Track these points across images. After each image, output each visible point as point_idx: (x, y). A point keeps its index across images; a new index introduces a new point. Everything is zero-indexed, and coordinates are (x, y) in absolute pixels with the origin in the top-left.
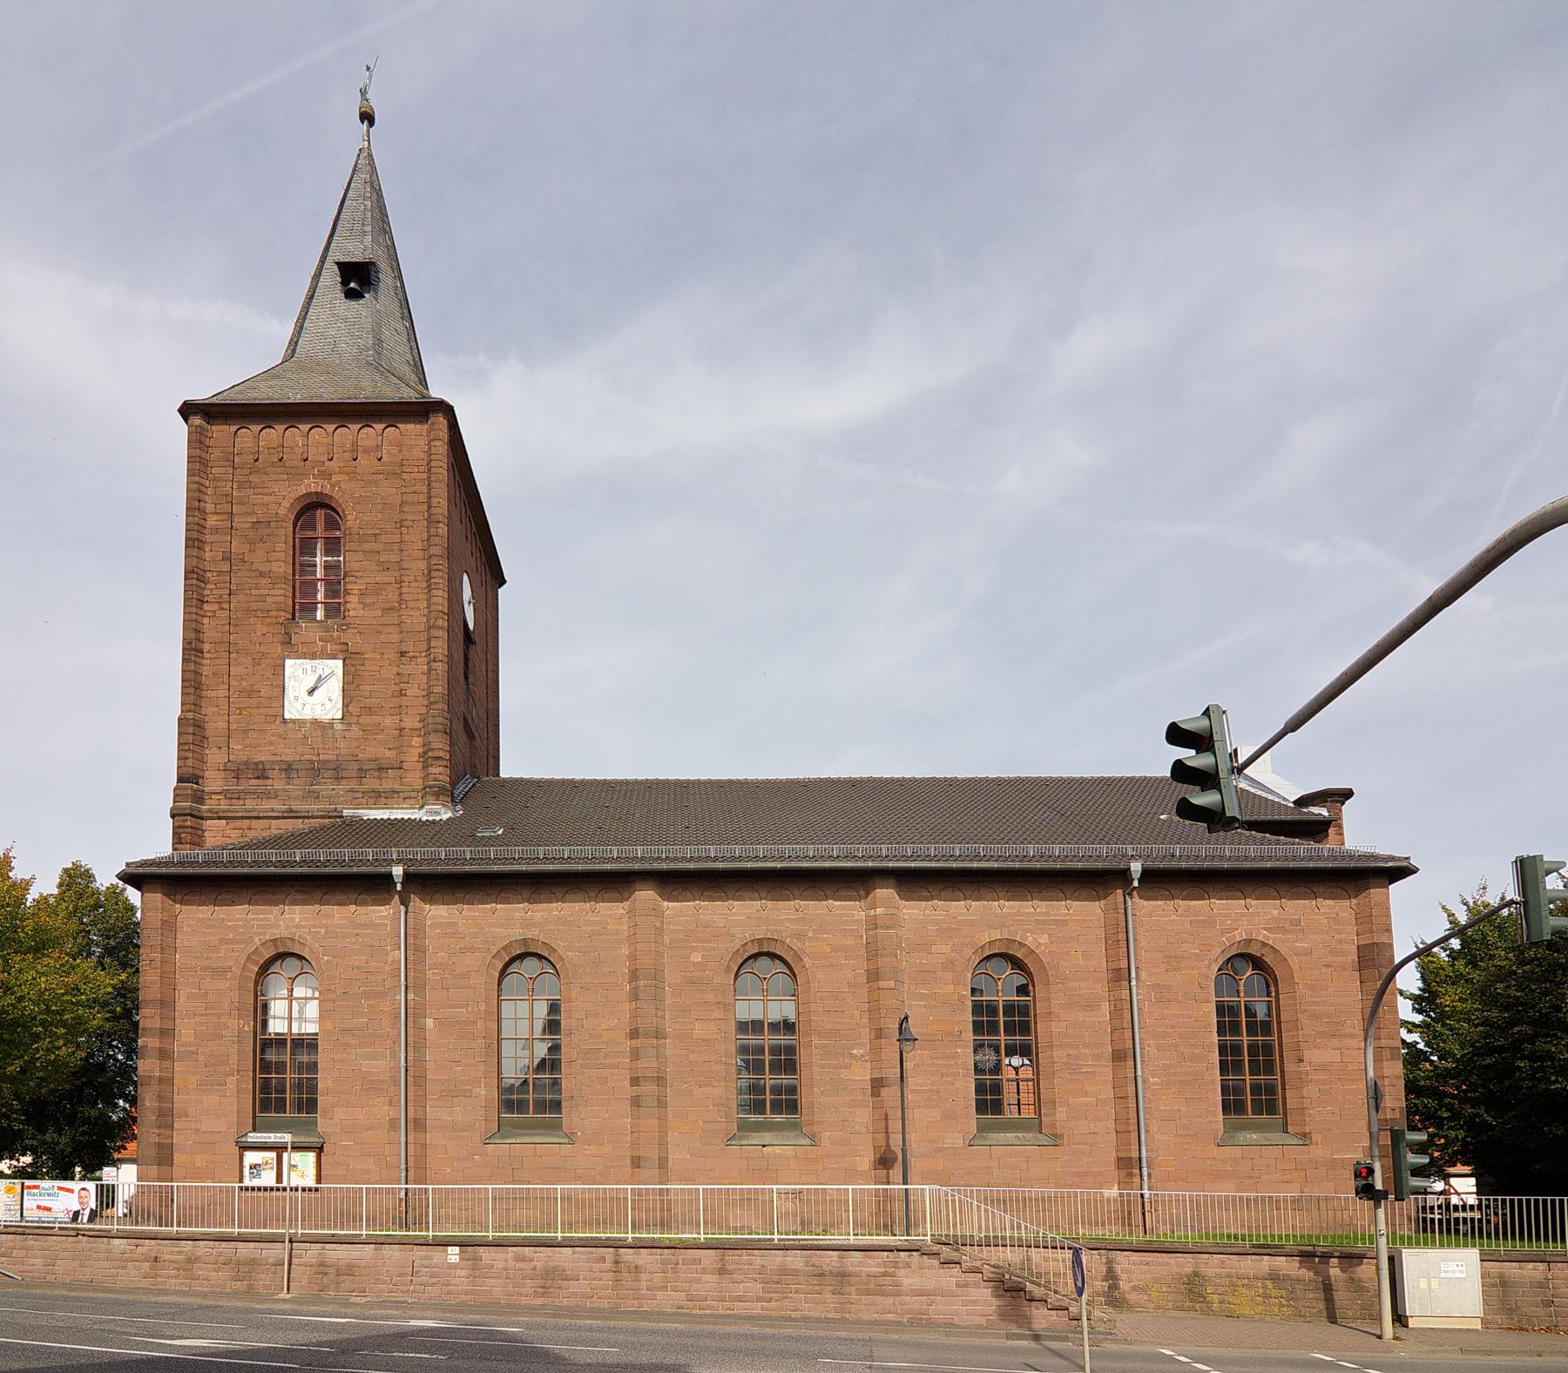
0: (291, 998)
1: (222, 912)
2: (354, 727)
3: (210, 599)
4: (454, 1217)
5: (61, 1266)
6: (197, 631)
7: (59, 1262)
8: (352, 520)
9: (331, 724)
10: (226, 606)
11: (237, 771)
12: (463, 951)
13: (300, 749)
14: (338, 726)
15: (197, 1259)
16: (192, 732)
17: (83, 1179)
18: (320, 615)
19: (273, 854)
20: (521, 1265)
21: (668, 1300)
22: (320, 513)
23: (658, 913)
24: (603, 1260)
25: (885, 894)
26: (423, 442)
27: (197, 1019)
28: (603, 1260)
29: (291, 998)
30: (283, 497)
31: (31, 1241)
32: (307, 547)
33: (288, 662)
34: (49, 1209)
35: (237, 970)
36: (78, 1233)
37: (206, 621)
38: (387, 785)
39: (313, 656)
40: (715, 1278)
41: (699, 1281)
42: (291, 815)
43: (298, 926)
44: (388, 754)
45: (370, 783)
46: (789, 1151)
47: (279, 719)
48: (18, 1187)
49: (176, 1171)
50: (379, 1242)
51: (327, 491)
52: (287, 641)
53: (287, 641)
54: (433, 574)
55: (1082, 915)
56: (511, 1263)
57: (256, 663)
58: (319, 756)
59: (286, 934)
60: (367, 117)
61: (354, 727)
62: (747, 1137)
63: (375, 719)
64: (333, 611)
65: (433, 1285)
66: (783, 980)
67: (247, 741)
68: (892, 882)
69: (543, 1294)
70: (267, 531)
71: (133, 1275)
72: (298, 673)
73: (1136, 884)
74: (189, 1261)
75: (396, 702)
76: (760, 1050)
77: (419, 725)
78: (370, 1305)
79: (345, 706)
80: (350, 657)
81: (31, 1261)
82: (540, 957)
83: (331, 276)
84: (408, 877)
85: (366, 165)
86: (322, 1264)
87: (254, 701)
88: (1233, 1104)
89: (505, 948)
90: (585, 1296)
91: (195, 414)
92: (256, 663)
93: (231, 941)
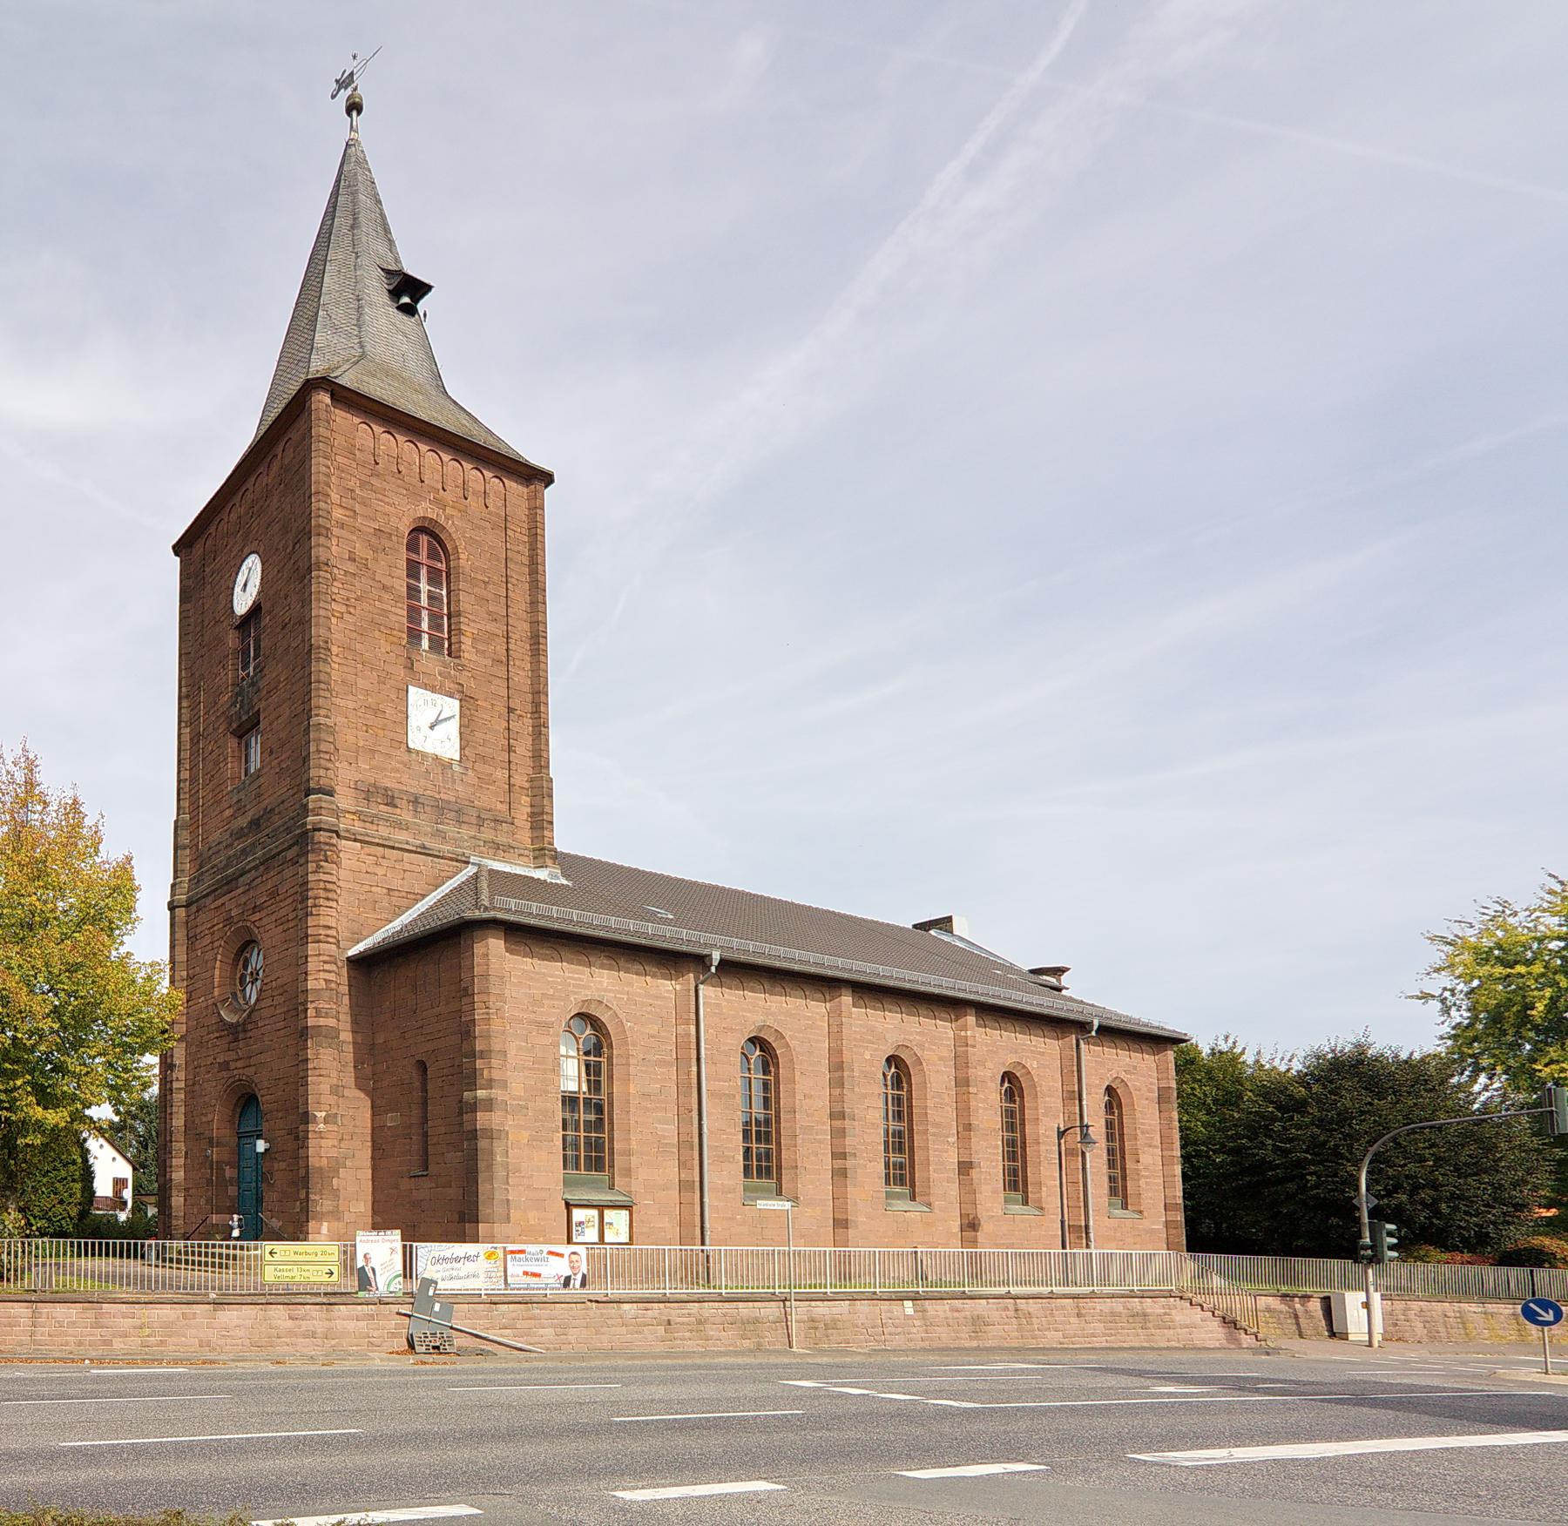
11: (369, 792)
14: (456, 768)
24: (1006, 1309)
31: (536, 1310)
34: (538, 1275)
39: (433, 690)
43: (605, 990)
44: (499, 806)
48: (500, 1253)
51: (442, 521)
55: (665, 989)
56: (949, 1314)
61: (470, 772)
63: (487, 769)
67: (374, 763)
70: (387, 544)
71: (652, 1338)
73: (713, 969)
74: (700, 1322)
81: (541, 1331)
87: (380, 722)
91: (326, 390)
93: (552, 997)
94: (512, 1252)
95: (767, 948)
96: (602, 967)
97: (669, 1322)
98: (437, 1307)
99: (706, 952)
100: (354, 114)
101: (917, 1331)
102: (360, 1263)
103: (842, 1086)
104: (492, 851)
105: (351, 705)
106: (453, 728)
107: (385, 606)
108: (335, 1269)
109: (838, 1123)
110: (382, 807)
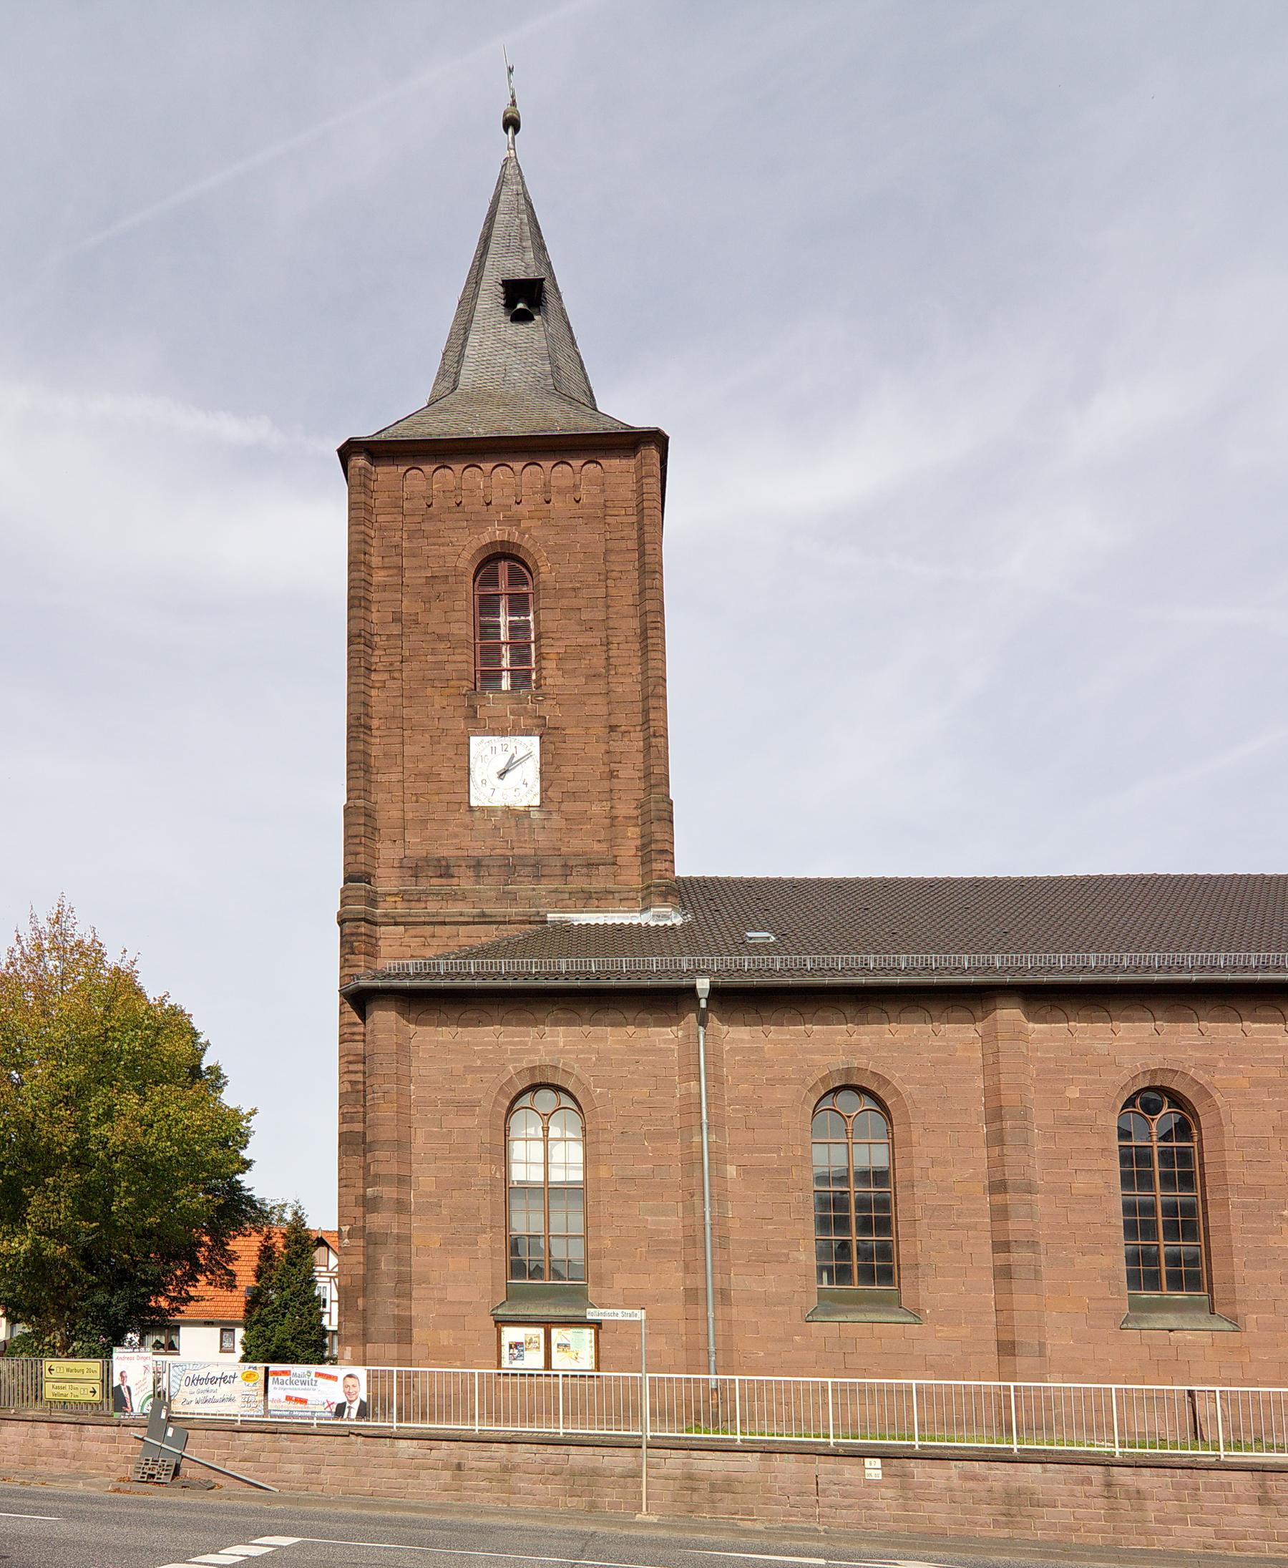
0: (546, 1139)
1: (466, 1034)
2: (555, 816)
3: (379, 667)
4: (770, 1413)
5: (326, 1475)
6: (366, 705)
7: (325, 1469)
8: (546, 572)
9: (527, 811)
10: (397, 675)
11: (415, 869)
12: (772, 1082)
13: (489, 842)
14: (535, 815)
15: (515, 1468)
16: (361, 823)
17: (354, 1363)
18: (506, 684)
19: (503, 965)
20: (970, 1485)
21: (1189, 1536)
22: (503, 567)
23: (1019, 1035)
24: (1089, 1481)
25: (1009, 1015)
26: (631, 480)
27: (439, 1164)
28: (1089, 1481)
29: (546, 1139)
30: (464, 548)
31: (284, 1441)
32: (487, 605)
33: (474, 741)
34: (304, 1401)
35: (487, 1105)
36: (351, 1433)
37: (374, 692)
38: (598, 884)
39: (503, 733)
40: (1255, 1509)
41: (1233, 1513)
42: (484, 920)
43: (562, 1052)
44: (596, 847)
45: (578, 882)
46: (1205, 1338)
47: (464, 807)
49: (417, 1351)
50: (768, 1450)
51: (516, 538)
52: (472, 715)
53: (472, 715)
54: (650, 633)
55: (955, 1037)
56: (956, 1482)
57: (434, 741)
58: (514, 853)
59: (547, 1060)
60: (512, 123)
61: (555, 816)
62: (1142, 1319)
63: (579, 806)
64: (520, 679)
65: (849, 1507)
66: (876, 1120)
67: (427, 833)
68: (1017, 1000)
69: (1007, 1525)
70: (443, 588)
71: (430, 1487)
72: (487, 753)
73: (703, 1004)
75: (605, 785)
76: (1149, 1209)
77: (636, 813)
78: (768, 1533)
79: (543, 790)
80: (548, 734)
81: (288, 1467)
82: (557, 1089)
83: (490, 300)
84: (715, 991)
85: (510, 177)
86: (690, 1477)
87: (433, 786)
88: (1142, 1271)
89: (823, 1080)
90: (1067, 1528)
92: (434, 741)
94: (275, 1373)
95: (933, 959)
96: (556, 1023)
97: (459, 1467)
98: (170, 1432)
99: (685, 982)
100: (511, 130)
101: (887, 1503)
102: (117, 1382)
103: (1002, 1143)
104: (580, 903)
105: (394, 777)
106: (530, 771)
107: (440, 658)
108: (97, 1388)
109: (998, 1198)
110: (435, 881)
